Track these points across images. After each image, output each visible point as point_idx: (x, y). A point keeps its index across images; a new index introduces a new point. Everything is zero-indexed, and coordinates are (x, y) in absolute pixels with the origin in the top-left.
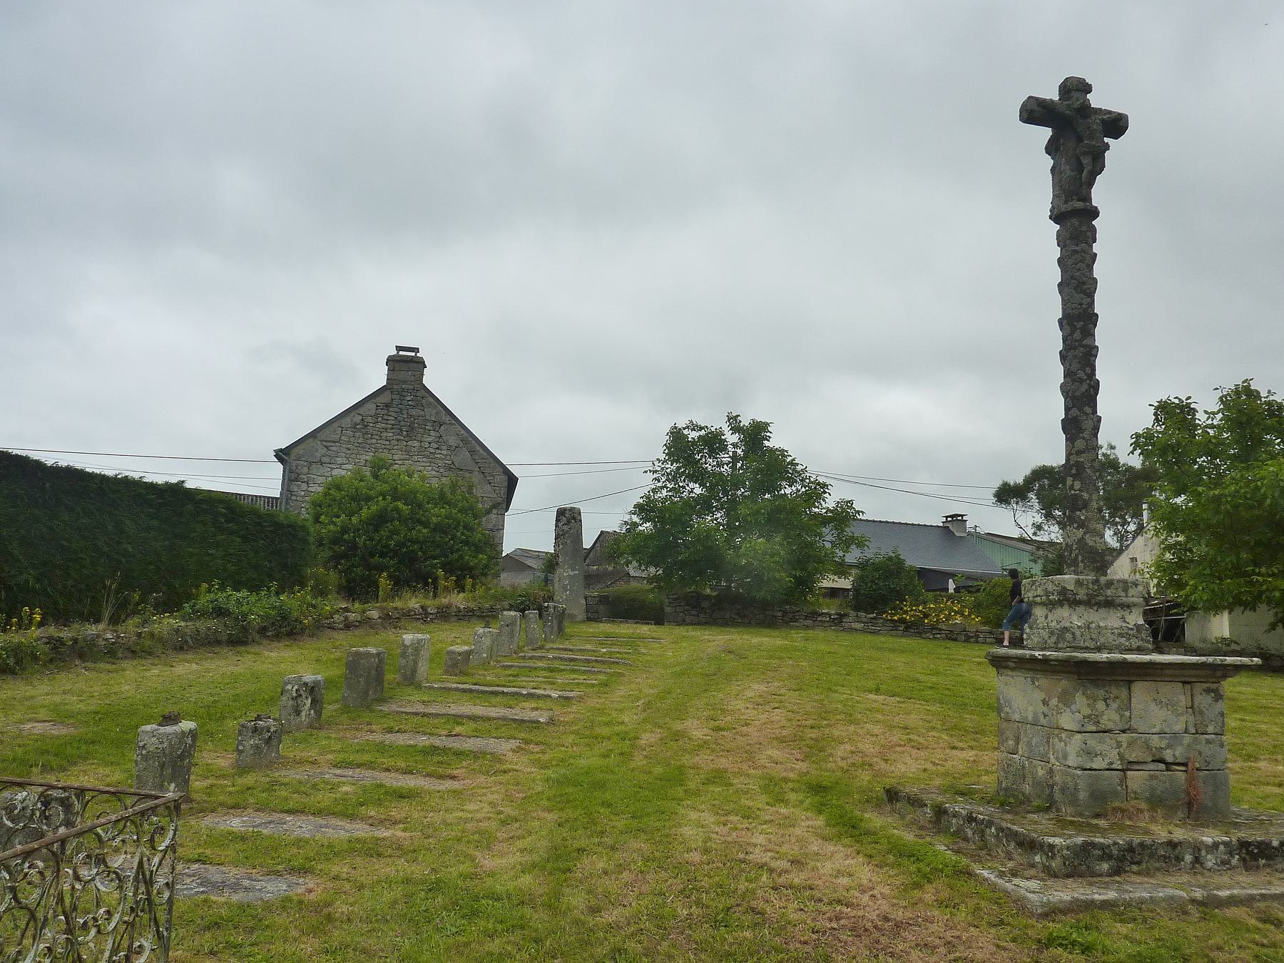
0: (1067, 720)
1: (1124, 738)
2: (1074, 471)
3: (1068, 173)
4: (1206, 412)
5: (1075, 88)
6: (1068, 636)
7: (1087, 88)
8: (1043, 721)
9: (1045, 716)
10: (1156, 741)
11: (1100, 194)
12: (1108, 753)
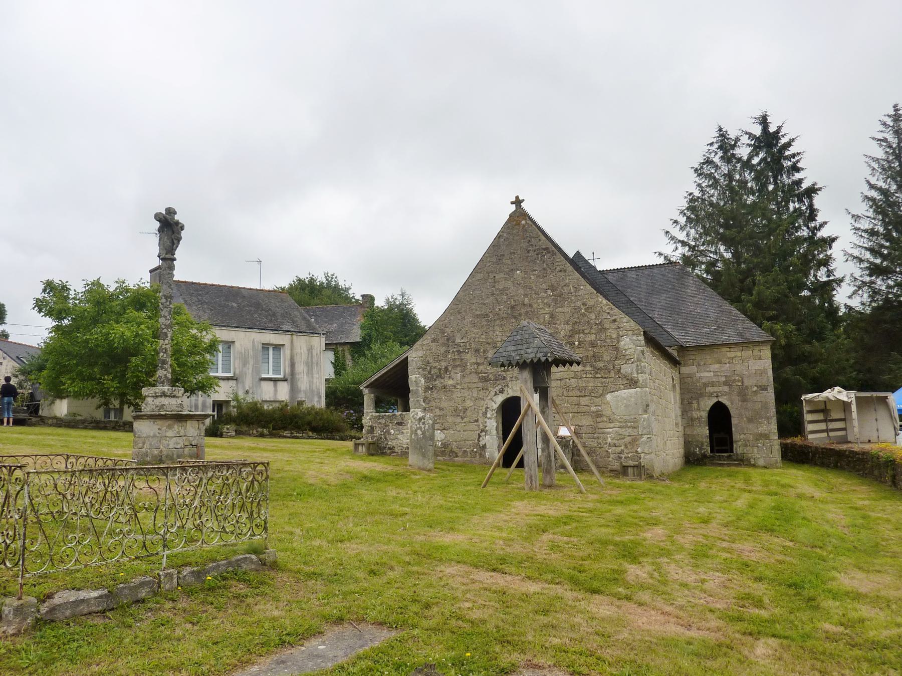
0: (170, 433)
1: (184, 438)
2: (164, 351)
3: (168, 243)
4: (75, 291)
5: (171, 212)
6: (165, 407)
7: (175, 213)
8: (158, 435)
9: (159, 433)
10: (191, 439)
11: (178, 254)
12: (181, 443)
